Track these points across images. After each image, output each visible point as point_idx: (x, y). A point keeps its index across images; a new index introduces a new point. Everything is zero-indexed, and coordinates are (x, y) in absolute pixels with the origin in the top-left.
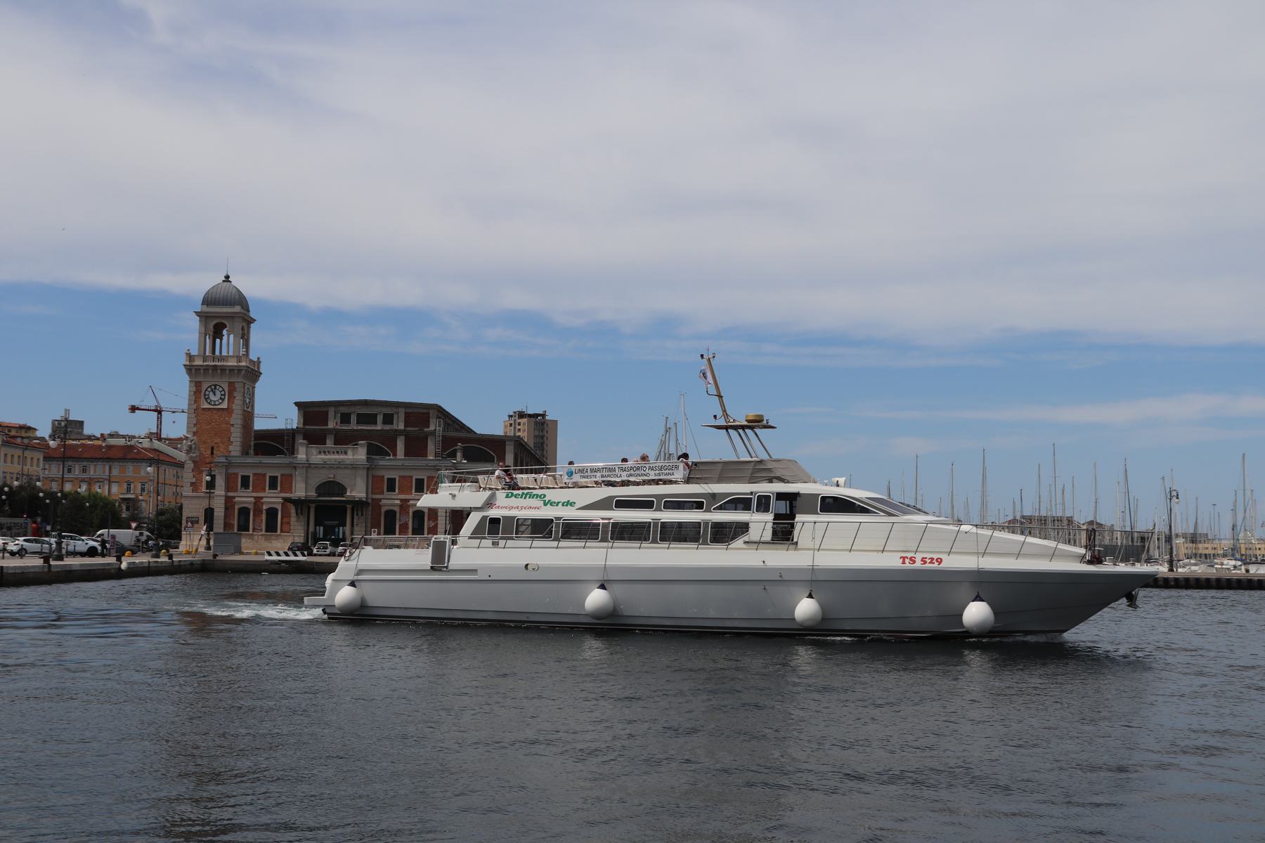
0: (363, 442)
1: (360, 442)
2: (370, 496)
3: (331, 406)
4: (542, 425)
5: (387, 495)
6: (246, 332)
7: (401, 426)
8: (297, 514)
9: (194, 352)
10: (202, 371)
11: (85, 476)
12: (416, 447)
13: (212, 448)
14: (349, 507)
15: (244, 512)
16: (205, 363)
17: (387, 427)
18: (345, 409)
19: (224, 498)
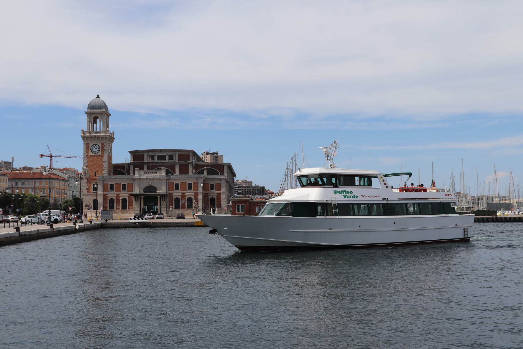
0: (164, 168)
1: (163, 168)
2: (168, 192)
3: (145, 152)
4: (217, 157)
5: (211, 191)
6: (107, 120)
7: (177, 161)
8: (136, 201)
9: (85, 130)
10: (89, 138)
11: (24, 186)
12: (184, 170)
13: (95, 173)
14: (159, 197)
15: (112, 201)
16: (90, 135)
17: (171, 161)
18: (152, 153)
19: (102, 195)
